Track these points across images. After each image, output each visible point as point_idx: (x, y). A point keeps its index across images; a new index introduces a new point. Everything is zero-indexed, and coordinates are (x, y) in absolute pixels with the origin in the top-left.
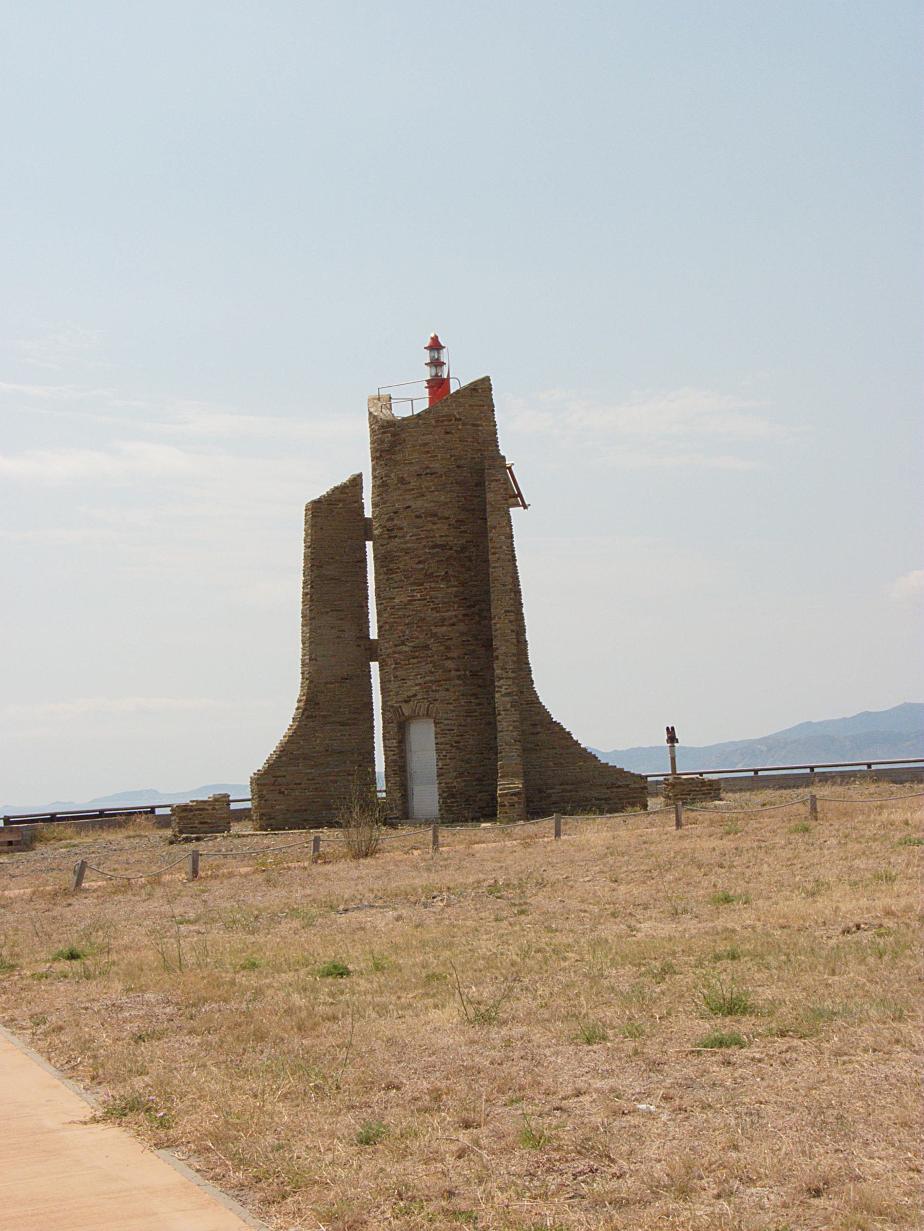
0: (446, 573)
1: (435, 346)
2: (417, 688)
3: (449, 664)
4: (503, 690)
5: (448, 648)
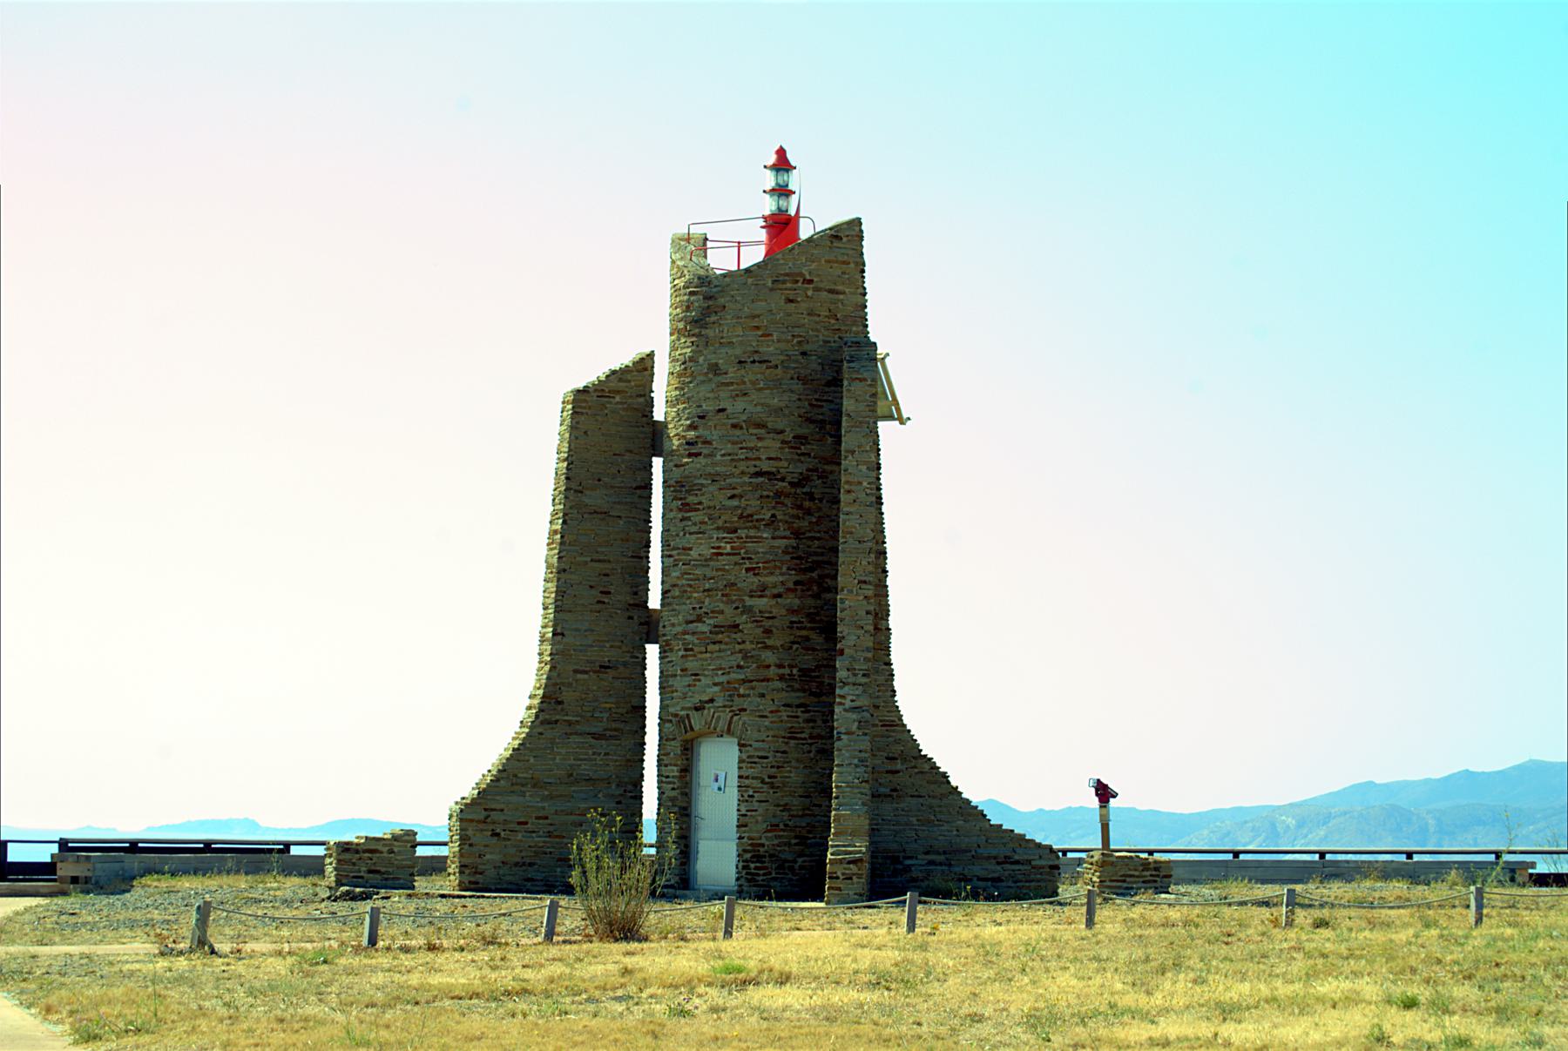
0: (773, 516)
1: (782, 164)
2: (716, 689)
3: (769, 657)
4: (848, 704)
5: (768, 632)
